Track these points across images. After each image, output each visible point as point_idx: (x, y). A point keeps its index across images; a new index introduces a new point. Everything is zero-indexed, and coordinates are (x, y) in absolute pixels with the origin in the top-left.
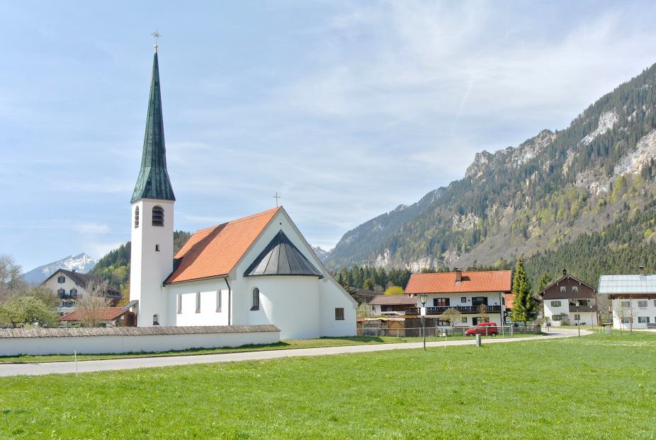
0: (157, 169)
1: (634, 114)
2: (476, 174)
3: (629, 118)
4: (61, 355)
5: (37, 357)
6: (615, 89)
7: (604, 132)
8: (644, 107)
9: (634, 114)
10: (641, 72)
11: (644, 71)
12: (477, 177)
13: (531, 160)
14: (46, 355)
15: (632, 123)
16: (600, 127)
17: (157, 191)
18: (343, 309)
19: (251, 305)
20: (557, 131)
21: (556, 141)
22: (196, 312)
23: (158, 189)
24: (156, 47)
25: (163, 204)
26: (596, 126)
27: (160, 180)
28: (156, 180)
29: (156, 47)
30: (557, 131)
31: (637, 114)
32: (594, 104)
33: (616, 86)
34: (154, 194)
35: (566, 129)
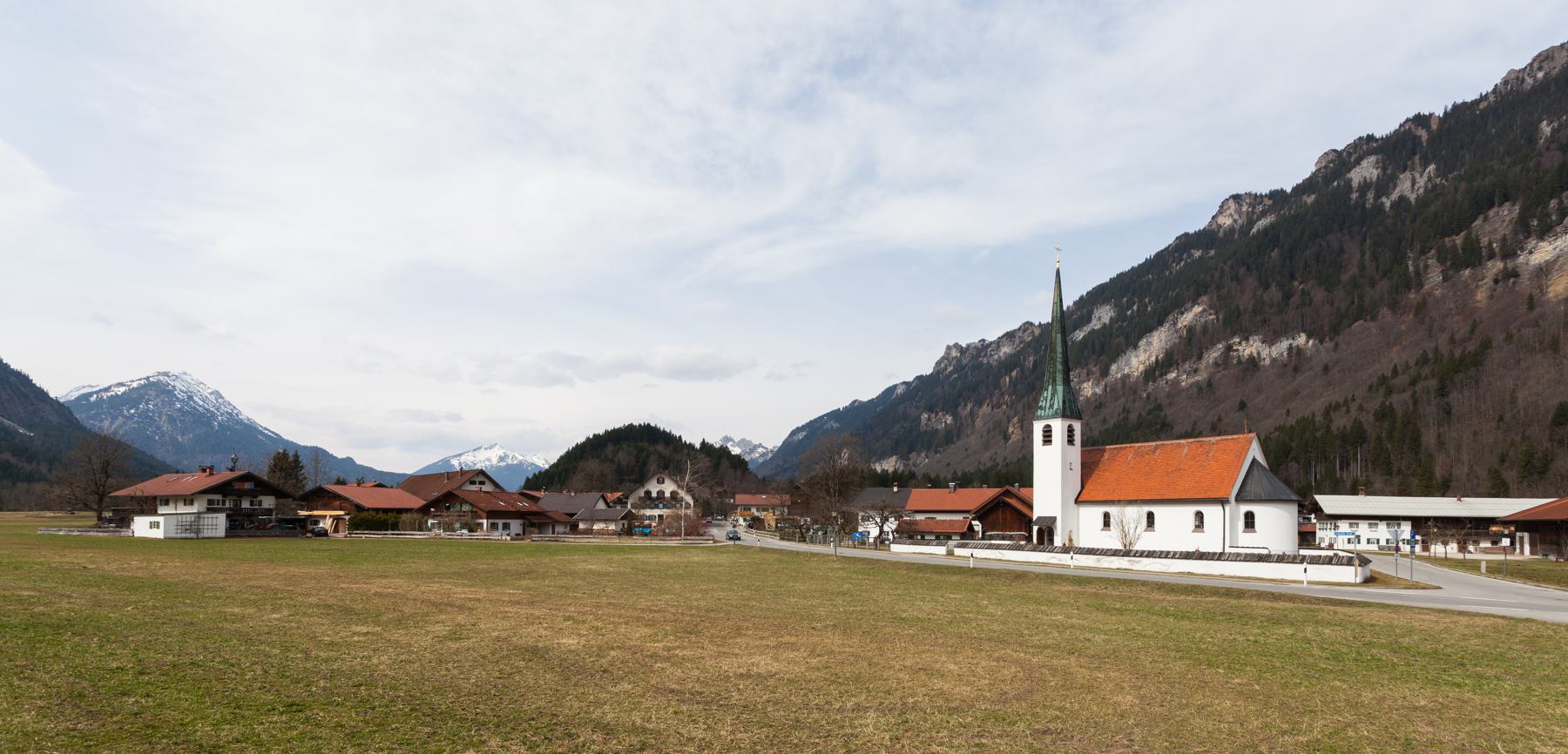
3: (1129, 312)
11: (1147, 259)
15: (1132, 317)
26: (1089, 320)
31: (1138, 309)
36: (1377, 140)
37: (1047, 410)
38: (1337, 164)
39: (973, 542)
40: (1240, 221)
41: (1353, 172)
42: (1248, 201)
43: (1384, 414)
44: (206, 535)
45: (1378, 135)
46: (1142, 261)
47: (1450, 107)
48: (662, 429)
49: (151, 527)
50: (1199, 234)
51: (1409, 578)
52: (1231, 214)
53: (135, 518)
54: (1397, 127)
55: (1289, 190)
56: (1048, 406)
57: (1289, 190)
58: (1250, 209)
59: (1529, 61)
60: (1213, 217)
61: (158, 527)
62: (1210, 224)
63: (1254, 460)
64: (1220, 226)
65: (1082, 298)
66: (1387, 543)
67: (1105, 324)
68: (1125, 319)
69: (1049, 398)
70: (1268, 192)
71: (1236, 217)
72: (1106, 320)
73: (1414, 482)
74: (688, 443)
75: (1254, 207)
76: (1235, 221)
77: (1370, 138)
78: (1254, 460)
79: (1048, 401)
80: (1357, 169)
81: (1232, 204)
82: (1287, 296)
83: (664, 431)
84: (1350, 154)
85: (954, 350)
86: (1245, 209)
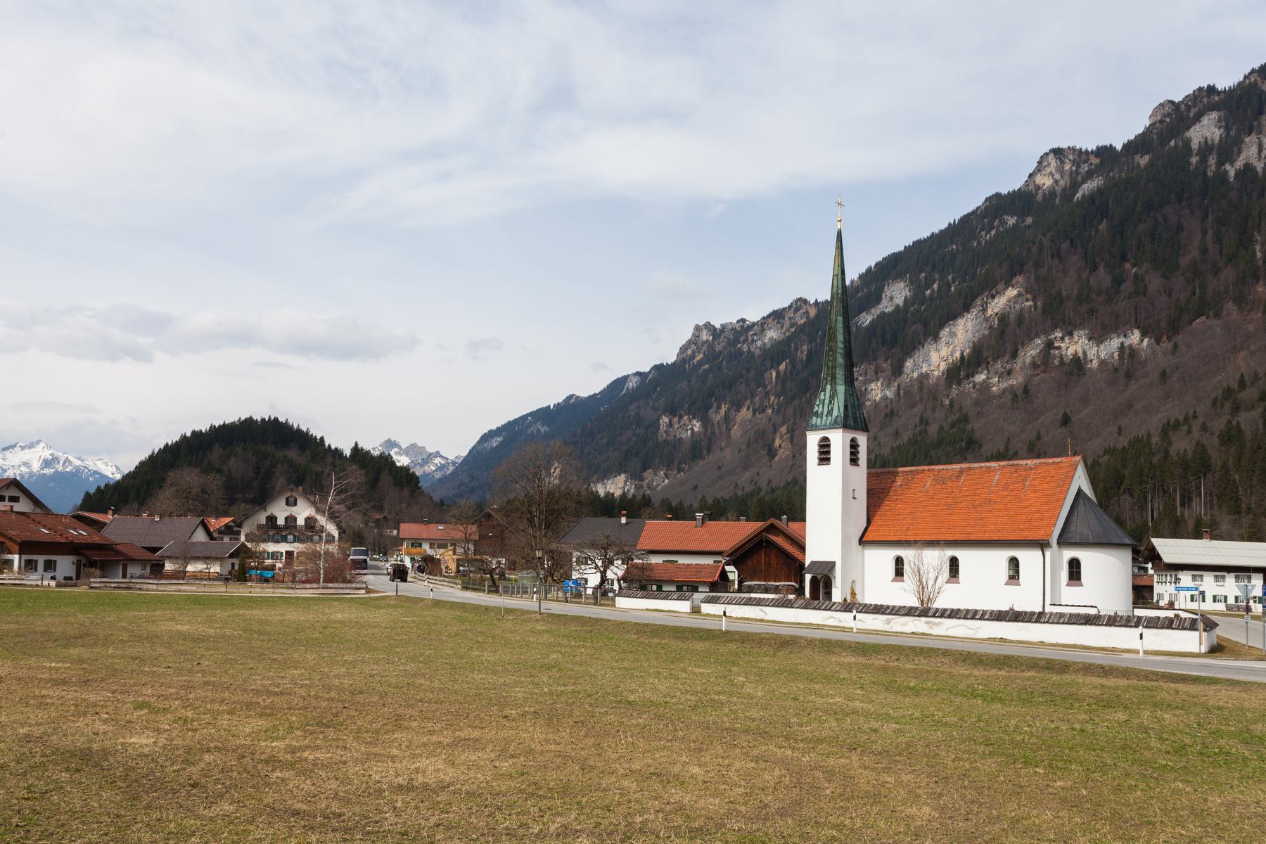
1: (935, 286)
3: (928, 292)
20: (816, 300)
30: (816, 300)
36: (1219, 93)
37: (825, 418)
39: (726, 595)
40: (1062, 183)
41: (1192, 130)
42: (1071, 157)
45: (1220, 87)
46: (944, 226)
50: (1015, 196)
52: (1051, 173)
55: (1119, 147)
56: (825, 413)
57: (1119, 147)
58: (1074, 168)
60: (1031, 176)
62: (1027, 184)
63: (1080, 491)
64: (1038, 187)
65: (869, 270)
66: (1236, 601)
67: (898, 306)
68: (923, 300)
69: (827, 402)
71: (1057, 177)
72: (899, 301)
75: (1079, 166)
76: (1056, 182)
77: (1211, 89)
78: (1080, 491)
80: (1197, 127)
81: (1052, 160)
82: (1118, 282)
84: (1188, 108)
85: (705, 332)
86: (1067, 167)
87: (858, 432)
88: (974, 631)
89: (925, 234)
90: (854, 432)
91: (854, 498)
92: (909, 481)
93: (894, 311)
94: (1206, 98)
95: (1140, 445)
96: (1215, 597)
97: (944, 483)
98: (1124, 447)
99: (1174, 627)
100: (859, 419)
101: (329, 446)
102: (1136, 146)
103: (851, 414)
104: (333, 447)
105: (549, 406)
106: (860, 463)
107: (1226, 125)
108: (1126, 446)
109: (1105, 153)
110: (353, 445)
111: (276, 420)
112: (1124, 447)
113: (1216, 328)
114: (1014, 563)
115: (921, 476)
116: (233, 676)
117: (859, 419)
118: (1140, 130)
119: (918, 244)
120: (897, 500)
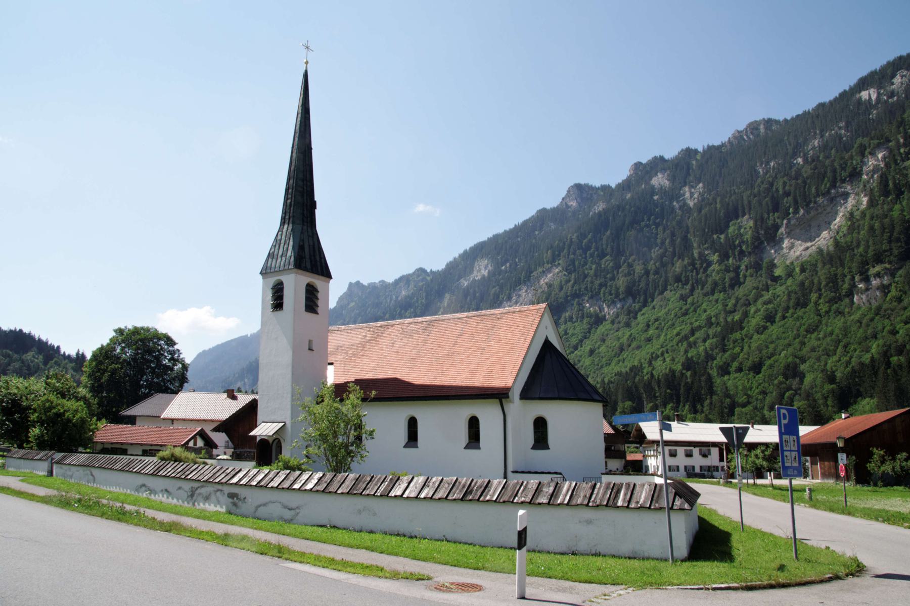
0: (309, 230)
1: (508, 265)
2: (348, 304)
3: (503, 268)
4: (613, 556)
5: (378, 536)
6: (488, 238)
7: (479, 277)
8: (517, 260)
9: (508, 265)
10: (513, 226)
11: (515, 225)
12: (349, 307)
13: (406, 297)
14: (619, 557)
15: (506, 272)
16: (475, 272)
17: (311, 261)
18: (479, 448)
19: (531, 441)
20: (431, 270)
21: (432, 280)
22: (406, 446)
23: (313, 258)
24: (307, 63)
25: (318, 281)
26: (471, 271)
27: (314, 248)
28: (309, 245)
29: (307, 63)
30: (431, 270)
31: (510, 266)
32: (468, 249)
33: (490, 235)
34: (309, 266)
35: (440, 269)
38: (643, 171)
39: (125, 457)
43: (689, 365)
44: (676, 500)
46: (512, 226)
47: (706, 147)
48: (37, 337)
49: (373, 438)
50: (554, 210)
51: (747, 497)
53: (366, 285)
54: (677, 154)
55: (613, 186)
57: (613, 186)
59: (745, 127)
61: (670, 467)
65: (465, 252)
66: (701, 470)
67: (484, 276)
68: (500, 272)
70: (600, 186)
73: (718, 420)
74: (67, 354)
79: (282, 245)
82: (617, 267)
83: (40, 340)
87: (317, 276)
88: (292, 512)
89: (500, 230)
90: (312, 275)
91: (309, 349)
92: (378, 336)
93: (481, 279)
94: (658, 163)
95: (636, 370)
96: (678, 470)
97: (411, 336)
98: (627, 372)
99: (620, 503)
100: (319, 263)
101: (64, 353)
102: (625, 186)
103: (307, 256)
104: (67, 354)
105: (247, 335)
106: (319, 312)
107: (672, 179)
108: (628, 371)
109: (605, 188)
110: (76, 352)
111: (21, 331)
112: (627, 372)
113: (689, 355)
114: (474, 423)
115: (390, 329)
116: (903, 519)
117: (319, 263)
118: (625, 178)
119: (496, 237)
120: (363, 355)
